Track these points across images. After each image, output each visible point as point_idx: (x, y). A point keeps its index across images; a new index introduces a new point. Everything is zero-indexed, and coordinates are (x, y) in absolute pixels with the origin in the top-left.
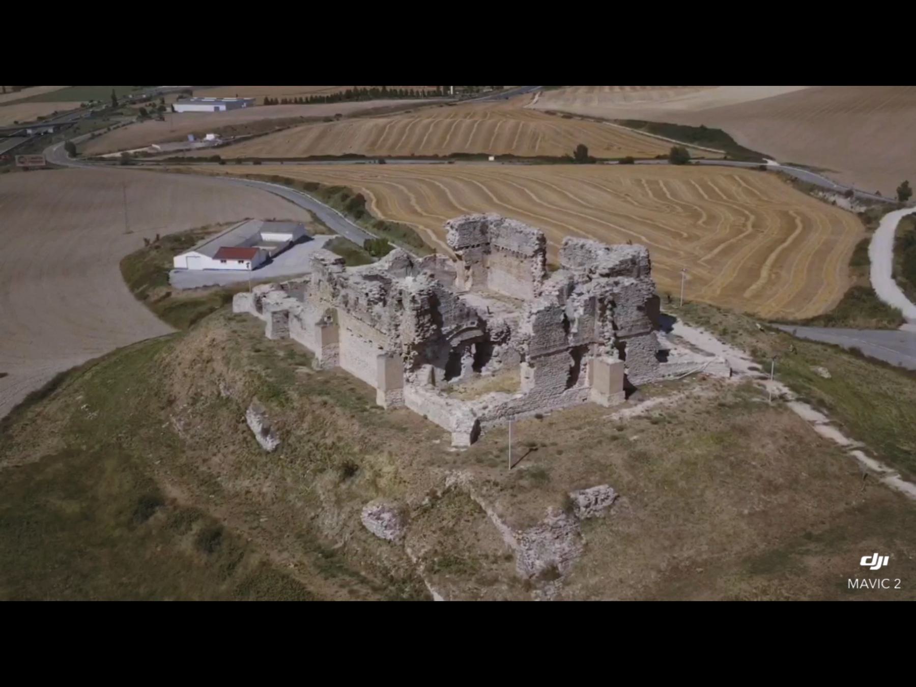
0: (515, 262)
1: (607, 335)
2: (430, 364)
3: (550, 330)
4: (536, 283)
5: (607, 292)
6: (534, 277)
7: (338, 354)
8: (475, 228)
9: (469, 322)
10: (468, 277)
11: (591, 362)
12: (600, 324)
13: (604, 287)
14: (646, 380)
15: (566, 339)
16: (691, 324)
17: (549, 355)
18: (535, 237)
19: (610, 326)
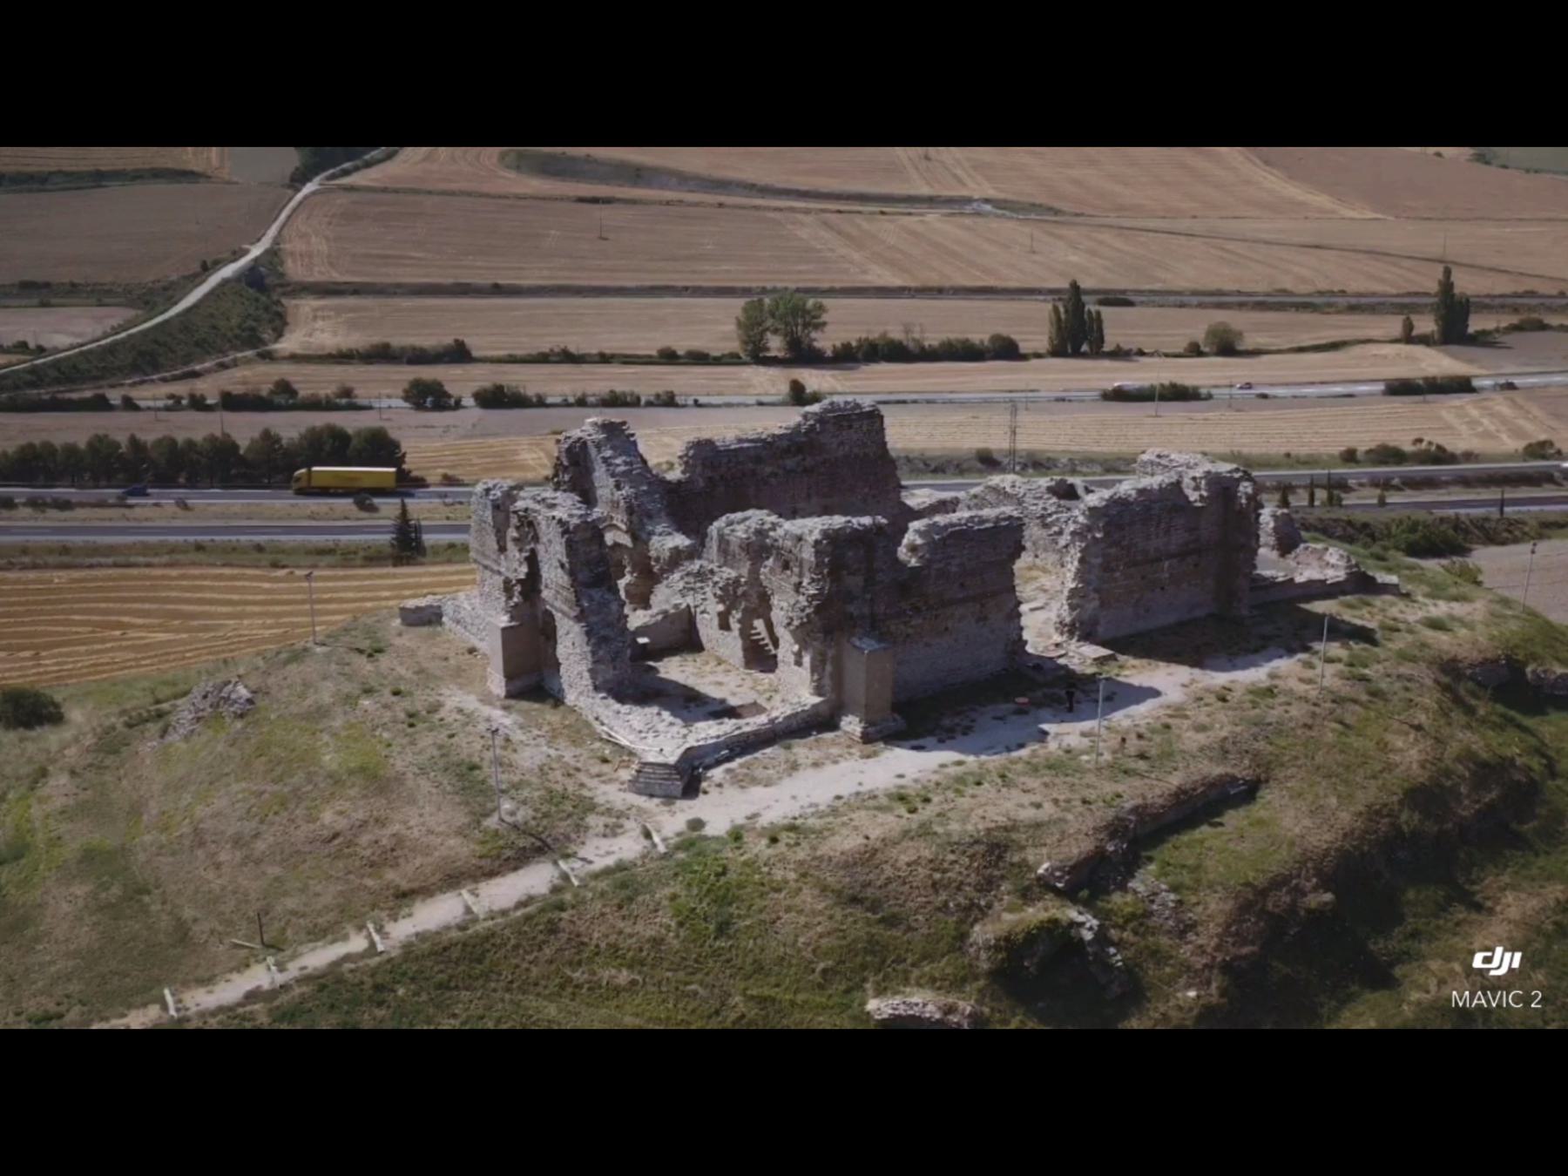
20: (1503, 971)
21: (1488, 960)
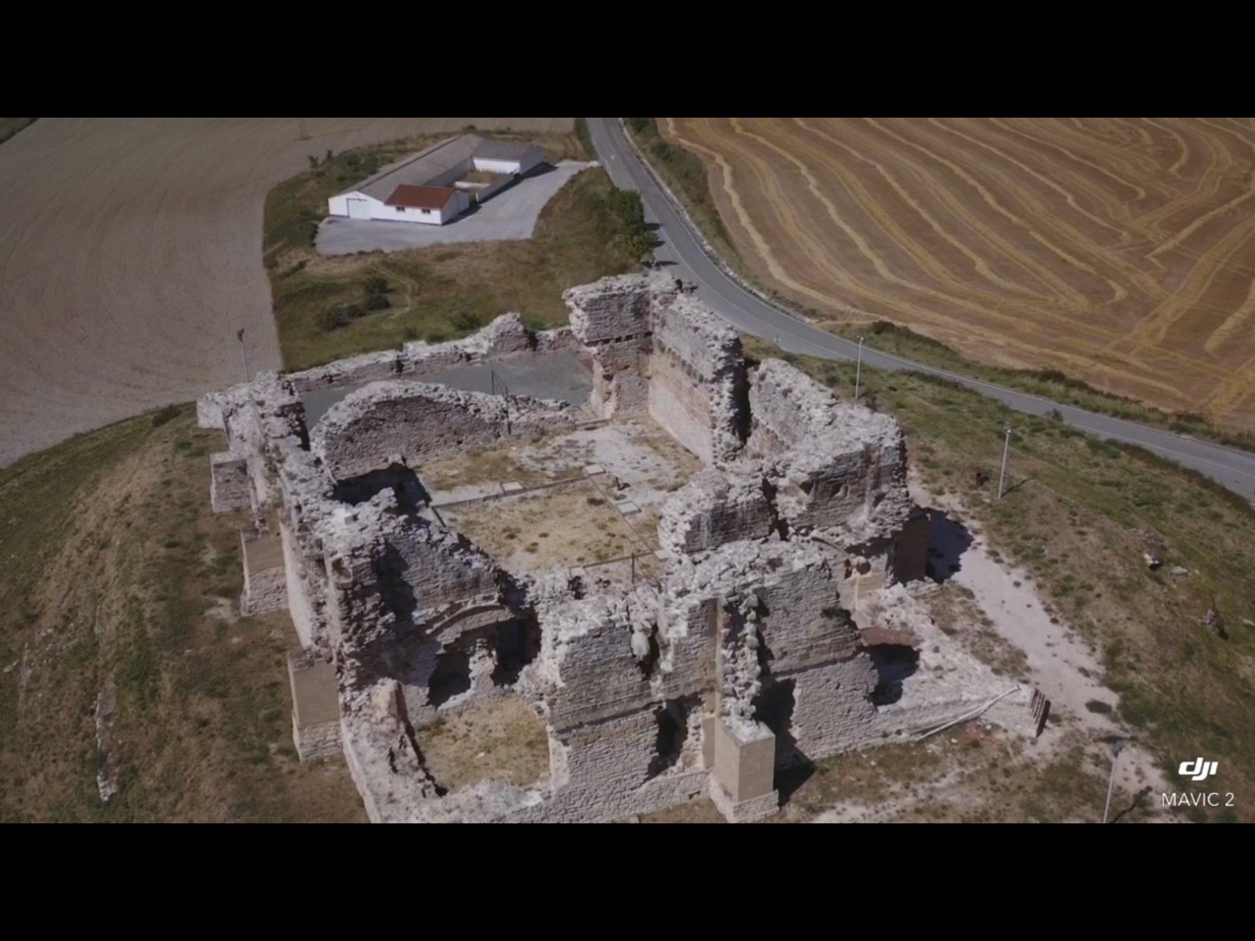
0: (687, 383)
1: (743, 676)
2: (393, 678)
3: (603, 674)
4: (716, 431)
5: (747, 585)
6: (714, 419)
7: (284, 587)
8: (621, 306)
9: (479, 597)
10: (610, 393)
11: (709, 724)
12: (728, 653)
13: (744, 573)
14: (841, 745)
15: (645, 686)
16: (1003, 556)
17: (602, 721)
18: (718, 345)
19: (752, 657)
20: (1203, 777)
21: (1191, 768)
